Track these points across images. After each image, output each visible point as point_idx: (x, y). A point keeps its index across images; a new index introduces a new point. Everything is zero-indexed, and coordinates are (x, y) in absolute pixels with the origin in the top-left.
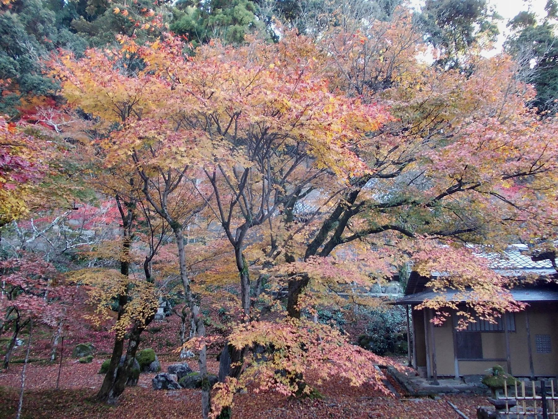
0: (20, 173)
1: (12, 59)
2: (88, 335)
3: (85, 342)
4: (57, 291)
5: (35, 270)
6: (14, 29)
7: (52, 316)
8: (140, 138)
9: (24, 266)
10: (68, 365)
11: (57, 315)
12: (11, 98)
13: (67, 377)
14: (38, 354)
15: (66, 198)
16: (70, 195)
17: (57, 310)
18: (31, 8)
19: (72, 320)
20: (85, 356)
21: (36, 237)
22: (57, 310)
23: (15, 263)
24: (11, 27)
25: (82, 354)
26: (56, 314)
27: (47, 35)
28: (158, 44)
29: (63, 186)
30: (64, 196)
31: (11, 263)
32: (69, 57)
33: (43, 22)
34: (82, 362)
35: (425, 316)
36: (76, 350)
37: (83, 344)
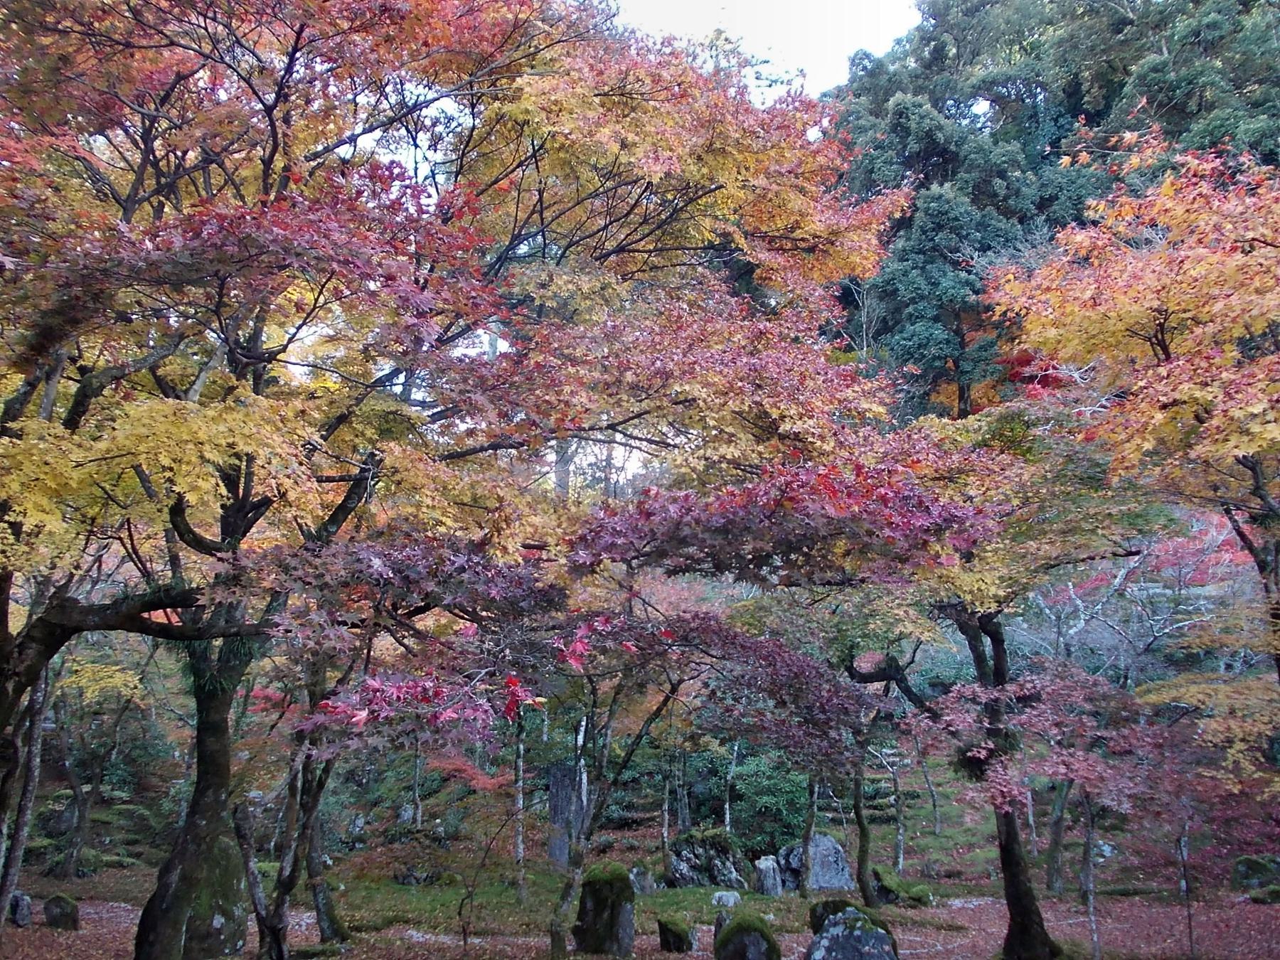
0: (960, 532)
1: (963, 274)
2: (1261, 835)
3: (1258, 852)
4: (1124, 737)
5: (1069, 696)
6: (951, 215)
7: (1120, 791)
8: (1164, 407)
9: (1049, 690)
10: (1221, 907)
11: (1130, 789)
12: (981, 348)
13: (1221, 932)
14: (1150, 876)
15: (1104, 535)
16: (1113, 527)
17: (1130, 778)
18: (973, 156)
19: (1166, 798)
20: (1261, 885)
21: (1087, 621)
22: (1130, 778)
23: (1029, 686)
24: (946, 213)
25: (1255, 881)
26: (1128, 786)
27: (1018, 193)
28: (1173, 184)
29: (1092, 511)
30: (1100, 532)
31: (1022, 687)
32: (1011, 277)
33: (1002, 175)
34: (1255, 901)
35: (299, 784)
36: (1237, 871)
37: (1254, 857)
